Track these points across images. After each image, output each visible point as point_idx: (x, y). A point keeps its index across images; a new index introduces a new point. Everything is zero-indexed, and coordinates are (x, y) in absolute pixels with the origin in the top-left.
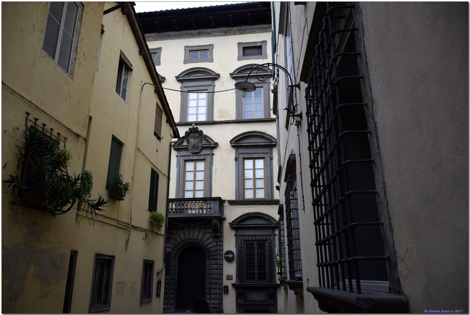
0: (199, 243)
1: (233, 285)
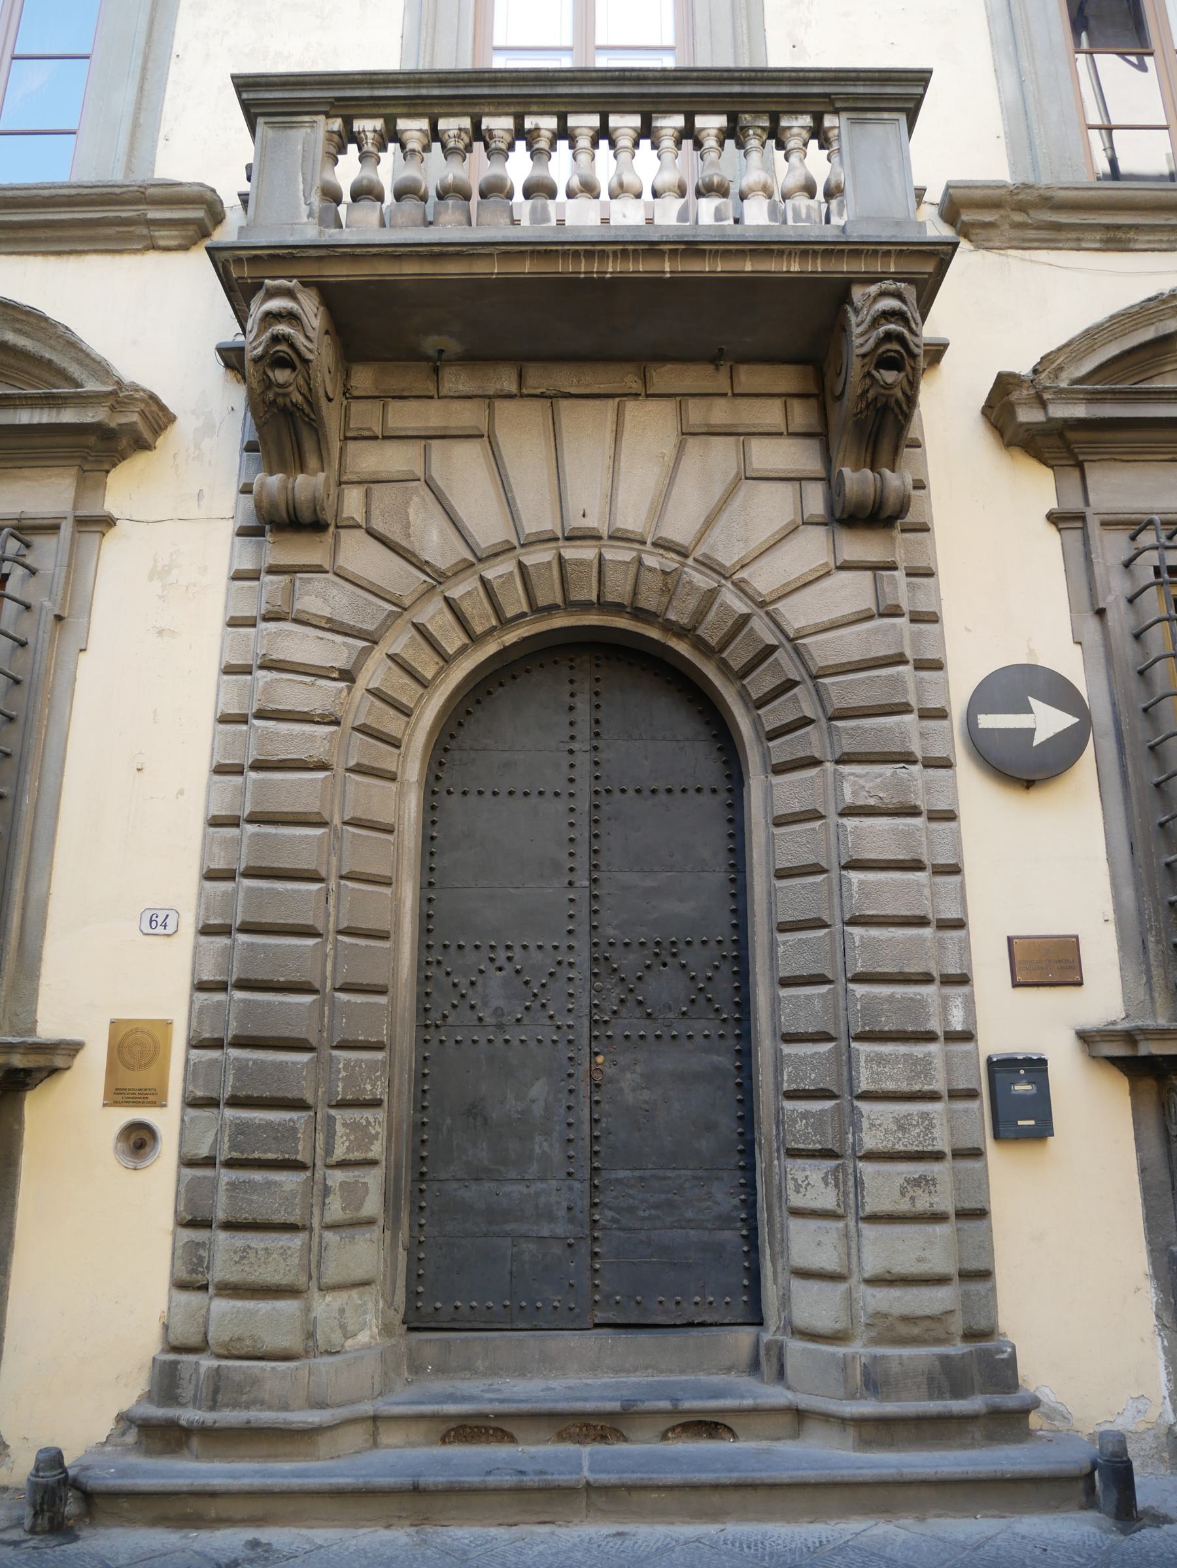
0: (670, 582)
1: (1102, 1046)
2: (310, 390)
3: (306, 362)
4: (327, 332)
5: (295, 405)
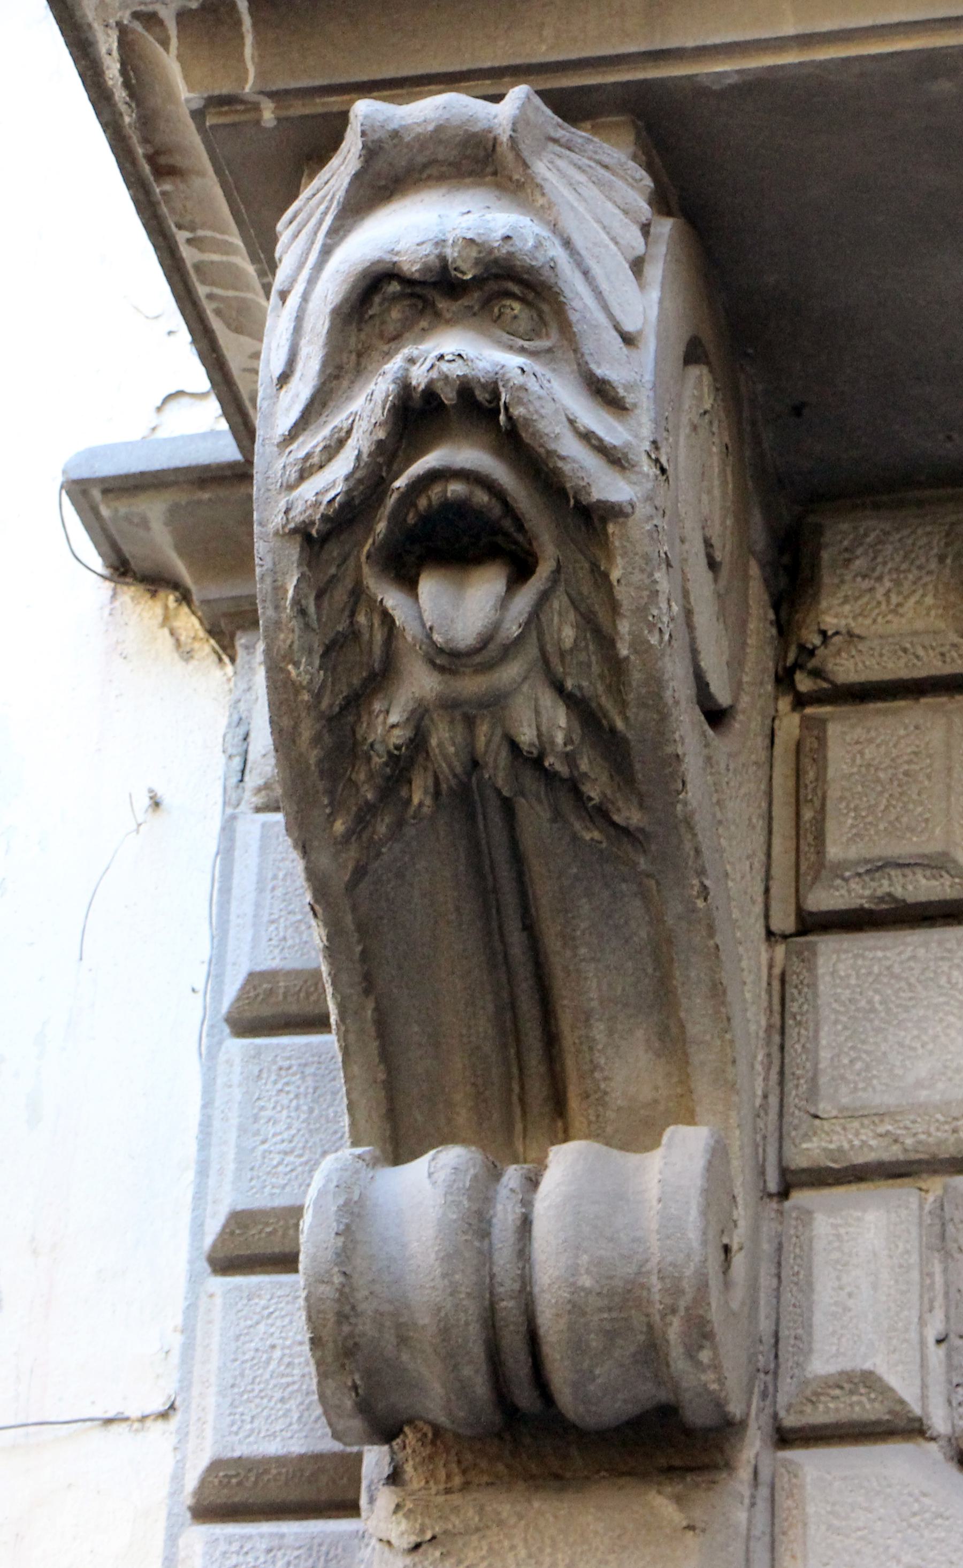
2: (616, 668)
3: (590, 521)
4: (693, 354)
5: (530, 761)
